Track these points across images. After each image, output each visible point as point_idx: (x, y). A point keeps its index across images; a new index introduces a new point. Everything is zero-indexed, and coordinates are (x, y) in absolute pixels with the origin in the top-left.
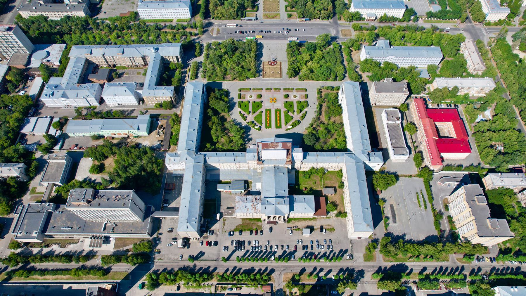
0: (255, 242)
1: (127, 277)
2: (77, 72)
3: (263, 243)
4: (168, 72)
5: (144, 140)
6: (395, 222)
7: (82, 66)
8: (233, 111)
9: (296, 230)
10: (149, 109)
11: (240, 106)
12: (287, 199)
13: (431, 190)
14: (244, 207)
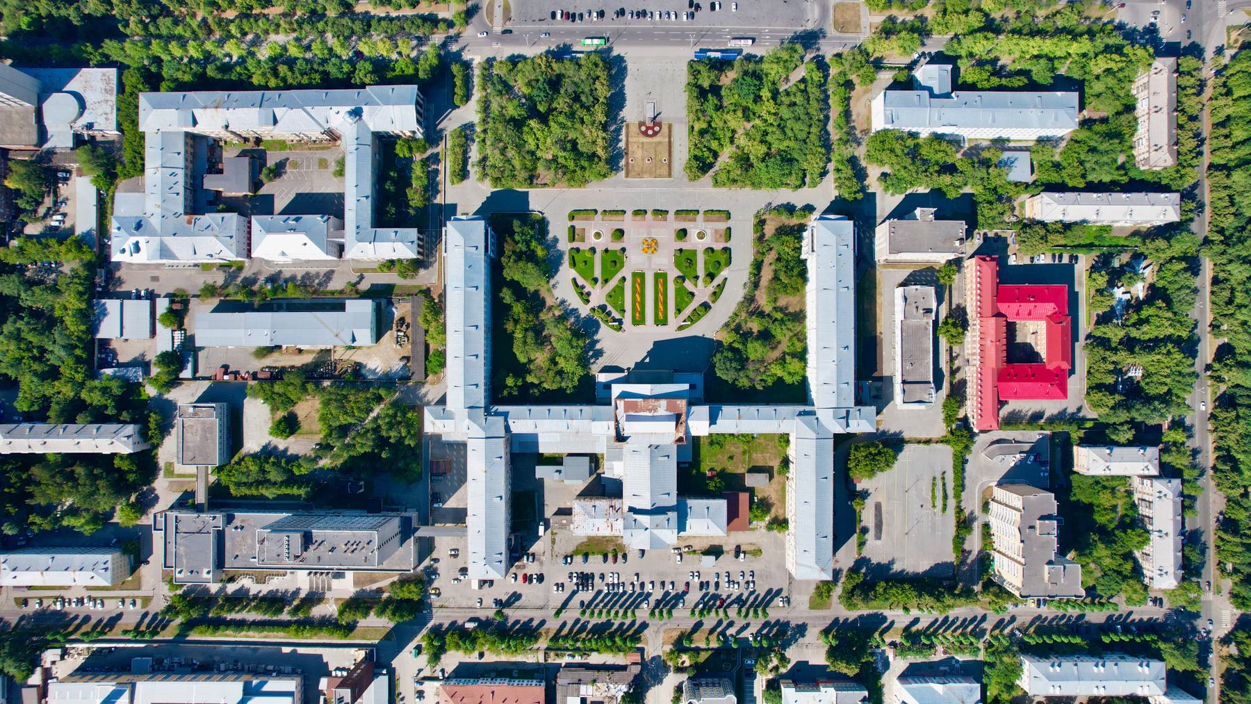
0: (612, 577)
1: (388, 637)
2: (173, 179)
3: (627, 577)
4: (395, 171)
5: (368, 355)
6: (878, 537)
7: (182, 157)
8: (557, 277)
9: (688, 553)
10: (367, 270)
11: (573, 264)
12: (673, 515)
13: (963, 470)
14: (591, 525)
